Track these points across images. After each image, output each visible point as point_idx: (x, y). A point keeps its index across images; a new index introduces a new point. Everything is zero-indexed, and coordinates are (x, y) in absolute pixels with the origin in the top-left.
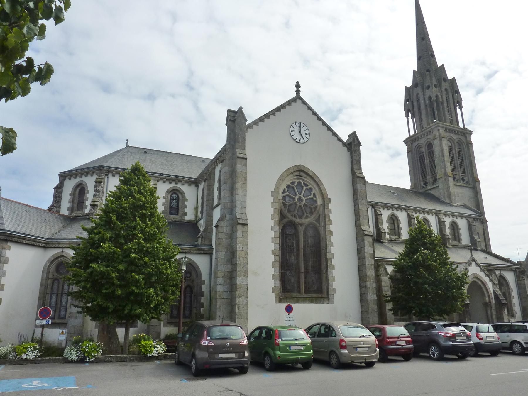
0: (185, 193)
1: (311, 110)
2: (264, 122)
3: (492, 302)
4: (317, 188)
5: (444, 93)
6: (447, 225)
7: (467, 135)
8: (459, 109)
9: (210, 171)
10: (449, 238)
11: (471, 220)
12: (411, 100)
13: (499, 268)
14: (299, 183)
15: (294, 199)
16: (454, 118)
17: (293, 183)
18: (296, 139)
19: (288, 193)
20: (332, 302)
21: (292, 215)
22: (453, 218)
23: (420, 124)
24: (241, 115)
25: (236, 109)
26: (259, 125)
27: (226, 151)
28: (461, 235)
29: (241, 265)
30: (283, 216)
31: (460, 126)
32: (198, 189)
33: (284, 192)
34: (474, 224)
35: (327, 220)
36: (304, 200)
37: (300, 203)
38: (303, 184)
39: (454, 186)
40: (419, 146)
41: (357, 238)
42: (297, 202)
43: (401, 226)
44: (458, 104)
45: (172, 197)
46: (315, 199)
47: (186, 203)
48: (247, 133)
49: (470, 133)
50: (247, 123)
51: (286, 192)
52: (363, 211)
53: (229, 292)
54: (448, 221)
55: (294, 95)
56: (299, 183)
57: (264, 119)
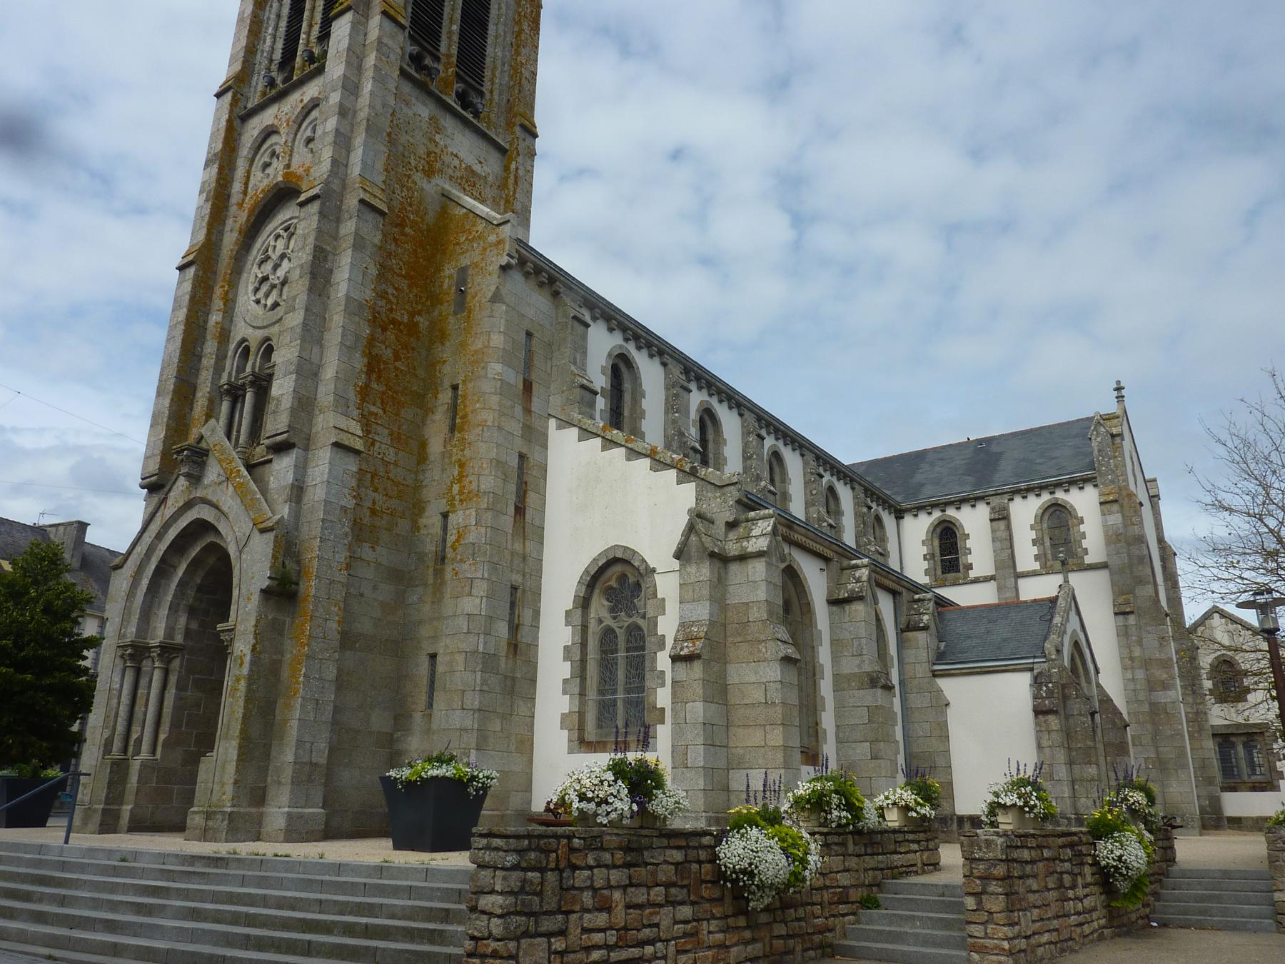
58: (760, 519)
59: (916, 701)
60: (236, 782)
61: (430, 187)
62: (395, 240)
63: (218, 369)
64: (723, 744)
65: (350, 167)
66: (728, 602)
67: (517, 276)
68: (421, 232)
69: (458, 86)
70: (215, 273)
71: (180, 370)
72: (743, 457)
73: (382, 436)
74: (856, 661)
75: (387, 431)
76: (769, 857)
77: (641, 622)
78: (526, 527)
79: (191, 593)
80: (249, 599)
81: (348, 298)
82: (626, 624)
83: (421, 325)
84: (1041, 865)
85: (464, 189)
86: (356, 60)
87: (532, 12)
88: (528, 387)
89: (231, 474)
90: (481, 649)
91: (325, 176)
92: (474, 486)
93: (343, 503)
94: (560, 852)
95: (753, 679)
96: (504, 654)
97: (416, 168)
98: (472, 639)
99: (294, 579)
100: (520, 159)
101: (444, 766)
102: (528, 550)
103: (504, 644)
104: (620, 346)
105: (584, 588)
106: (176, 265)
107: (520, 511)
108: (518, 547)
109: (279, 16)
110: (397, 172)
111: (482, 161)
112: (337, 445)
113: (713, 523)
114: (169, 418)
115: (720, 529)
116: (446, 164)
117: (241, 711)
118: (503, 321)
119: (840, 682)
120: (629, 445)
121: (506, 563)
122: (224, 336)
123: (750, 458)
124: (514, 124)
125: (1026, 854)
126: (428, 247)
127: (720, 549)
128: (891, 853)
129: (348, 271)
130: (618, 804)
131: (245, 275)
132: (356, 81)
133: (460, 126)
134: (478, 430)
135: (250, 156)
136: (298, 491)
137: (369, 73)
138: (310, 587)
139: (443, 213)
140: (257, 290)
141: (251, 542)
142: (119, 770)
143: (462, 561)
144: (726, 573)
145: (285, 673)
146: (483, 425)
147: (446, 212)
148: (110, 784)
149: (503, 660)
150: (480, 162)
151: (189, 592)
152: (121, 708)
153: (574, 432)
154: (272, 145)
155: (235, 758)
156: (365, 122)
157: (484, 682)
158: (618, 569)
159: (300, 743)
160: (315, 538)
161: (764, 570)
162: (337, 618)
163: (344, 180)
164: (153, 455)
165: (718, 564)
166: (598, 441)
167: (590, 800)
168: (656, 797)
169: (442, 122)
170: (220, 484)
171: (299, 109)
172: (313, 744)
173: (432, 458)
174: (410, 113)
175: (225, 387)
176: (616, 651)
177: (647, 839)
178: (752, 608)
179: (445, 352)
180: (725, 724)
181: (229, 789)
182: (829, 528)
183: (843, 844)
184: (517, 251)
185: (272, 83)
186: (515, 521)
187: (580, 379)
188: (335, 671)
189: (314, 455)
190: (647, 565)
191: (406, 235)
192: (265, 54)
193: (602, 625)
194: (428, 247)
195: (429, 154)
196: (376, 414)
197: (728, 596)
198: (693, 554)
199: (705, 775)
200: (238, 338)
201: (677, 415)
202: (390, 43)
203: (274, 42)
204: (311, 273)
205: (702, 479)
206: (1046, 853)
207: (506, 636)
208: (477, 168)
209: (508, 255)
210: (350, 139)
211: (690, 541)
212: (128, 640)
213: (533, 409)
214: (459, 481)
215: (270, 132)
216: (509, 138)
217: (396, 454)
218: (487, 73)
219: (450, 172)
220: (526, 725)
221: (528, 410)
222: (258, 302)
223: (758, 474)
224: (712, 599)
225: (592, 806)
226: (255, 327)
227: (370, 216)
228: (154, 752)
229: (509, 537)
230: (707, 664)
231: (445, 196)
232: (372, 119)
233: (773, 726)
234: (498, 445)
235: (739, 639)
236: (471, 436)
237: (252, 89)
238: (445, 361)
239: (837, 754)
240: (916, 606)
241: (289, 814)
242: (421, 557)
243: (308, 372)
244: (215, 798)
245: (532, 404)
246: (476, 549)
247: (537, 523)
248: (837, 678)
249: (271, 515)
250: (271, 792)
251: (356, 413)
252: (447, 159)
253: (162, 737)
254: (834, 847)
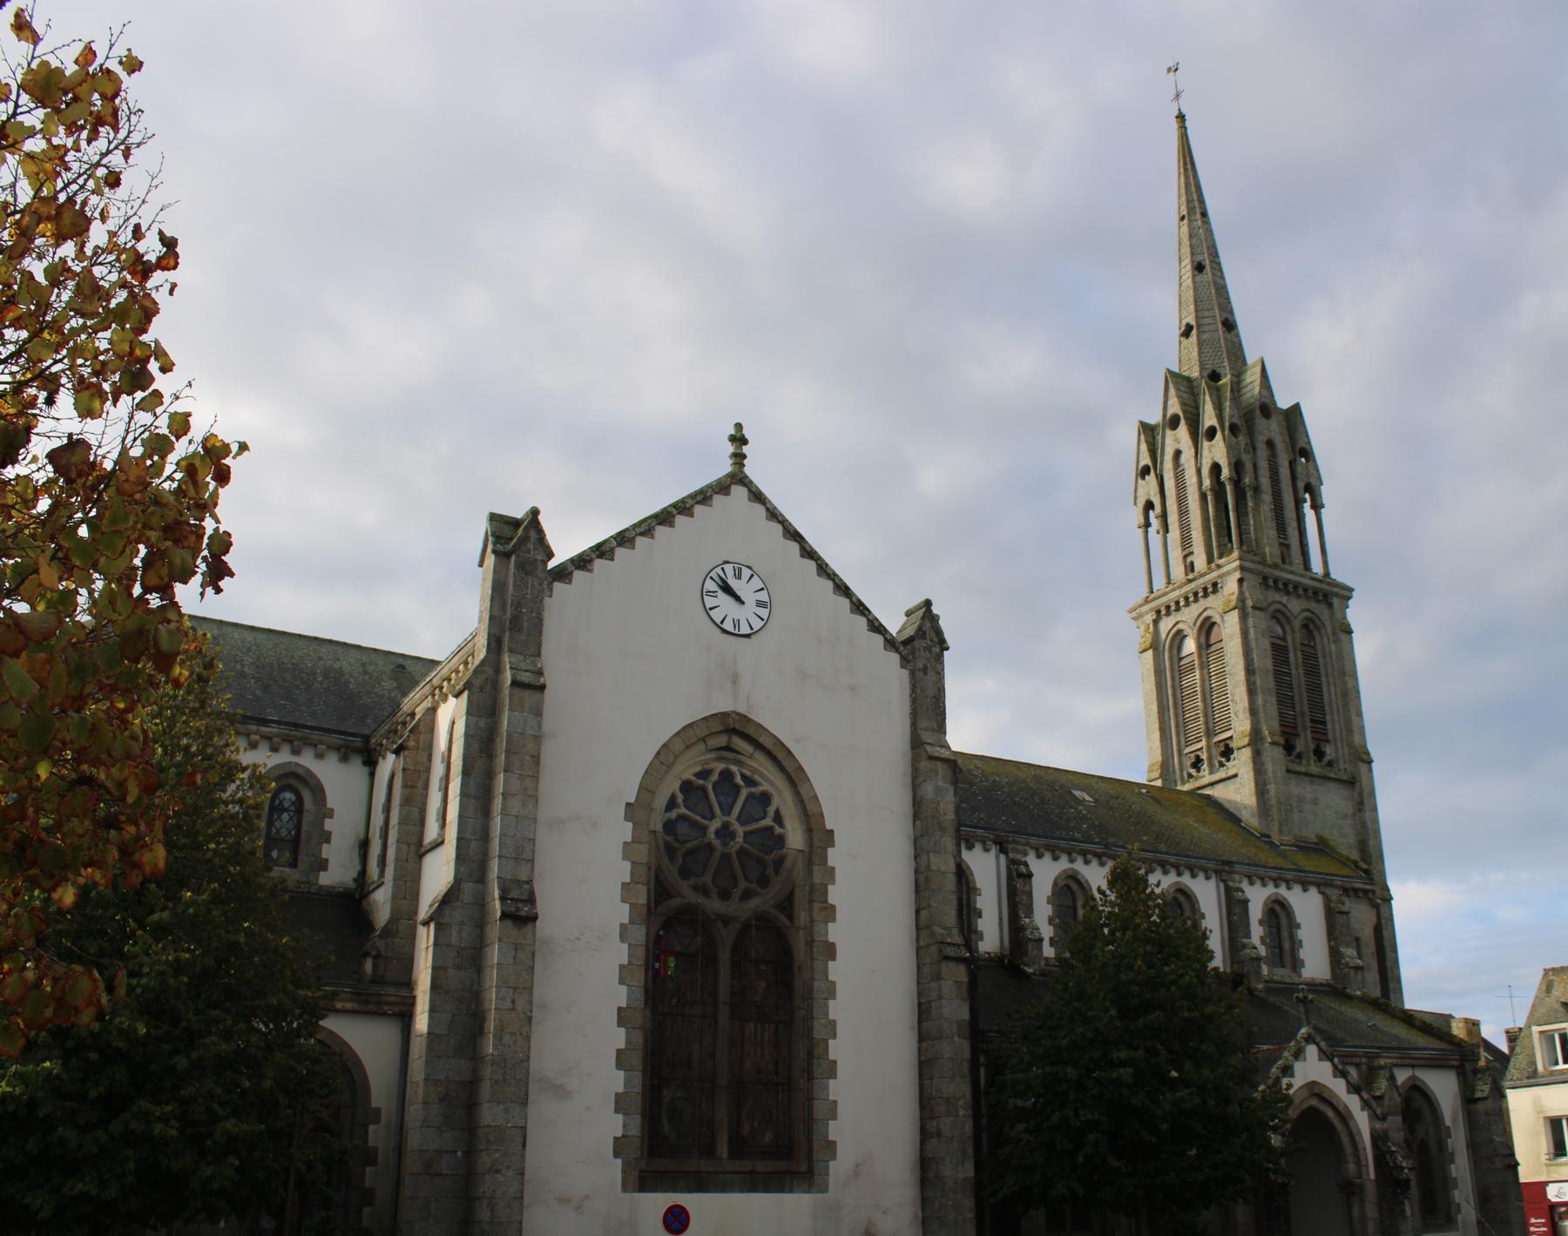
0: (326, 788)
1: (780, 522)
2: (612, 559)
3: (1365, 1177)
4: (788, 795)
5: (1263, 453)
6: (1256, 912)
7: (1336, 601)
8: (1312, 512)
9: (417, 717)
10: (1258, 959)
11: (1334, 894)
12: (1155, 470)
13: (1407, 1061)
14: (726, 775)
15: (704, 829)
16: (1294, 541)
17: (704, 774)
18: (722, 622)
19: (683, 810)
20: (824, 1189)
21: (696, 888)
22: (1277, 886)
23: (1185, 557)
24: (533, 534)
25: (518, 512)
26: (595, 571)
27: (473, 655)
28: (1301, 947)
29: (505, 1060)
30: (660, 891)
31: (1315, 570)
32: (372, 774)
33: (672, 804)
34: (1345, 909)
35: (816, 906)
36: (742, 834)
37: (725, 844)
38: (738, 780)
39: (1289, 775)
40: (1208, 618)
41: (918, 967)
42: (717, 843)
44: (1307, 496)
45: (277, 802)
46: (778, 830)
47: (328, 824)
48: (551, 596)
49: (1345, 593)
50: (552, 564)
51: (678, 807)
52: (943, 873)
53: (459, 1154)
54: (1257, 897)
55: (726, 467)
56: (726, 775)
57: (612, 550)
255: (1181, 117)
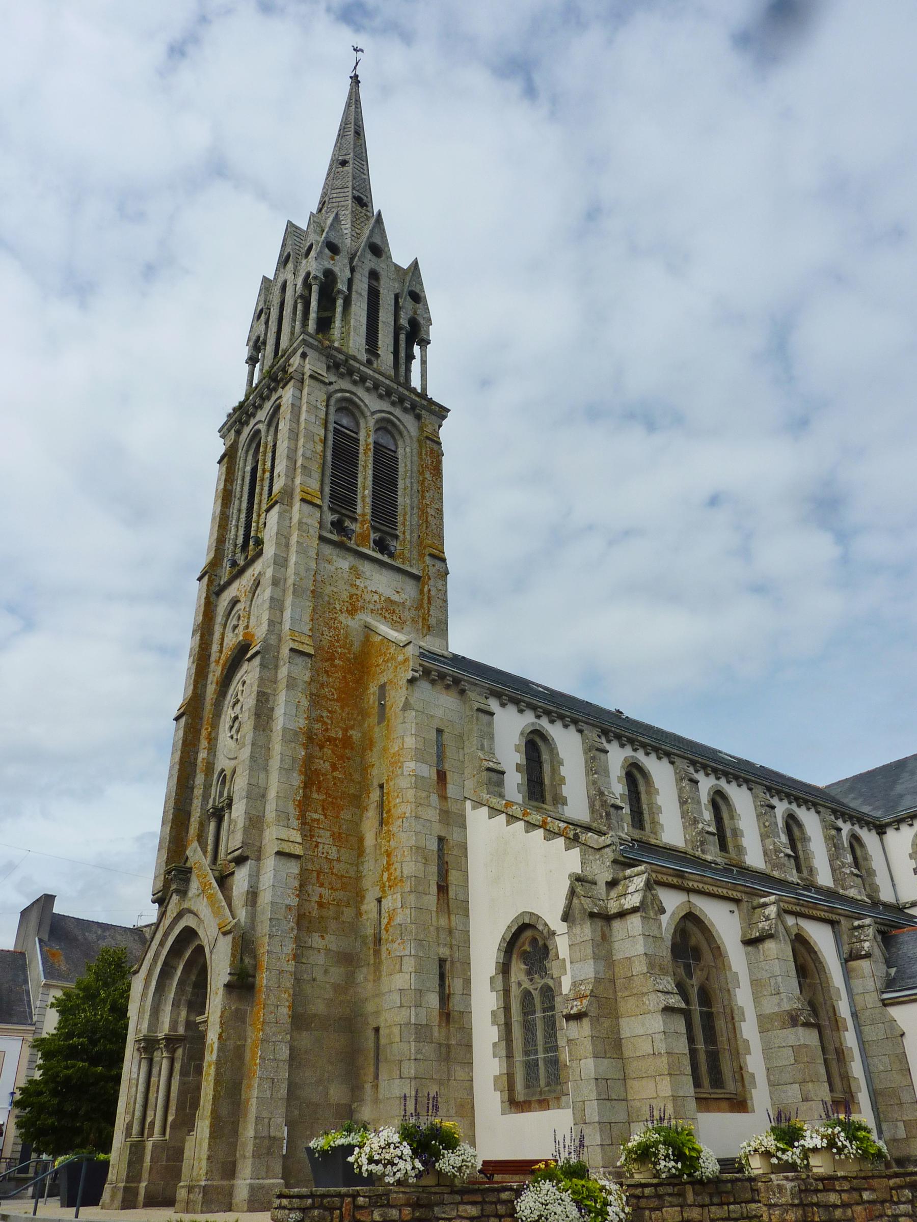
43: (564, 771)
49: (441, 412)
58: (635, 876)
59: (872, 1033)
60: (209, 1158)
61: (353, 623)
62: (327, 672)
63: (206, 796)
64: (622, 1098)
65: (283, 624)
66: (614, 958)
67: (424, 685)
68: (349, 660)
69: (373, 536)
70: (201, 719)
71: (177, 802)
72: (680, 802)
73: (324, 837)
74: (775, 999)
75: (328, 834)
76: (559, 1209)
77: (551, 983)
78: (450, 904)
79: (189, 989)
80: (217, 993)
81: (285, 730)
82: (539, 986)
83: (354, 737)
84: (859, 1209)
85: (385, 617)
86: (284, 540)
87: (433, 462)
88: (442, 777)
89: (205, 887)
90: (413, 1021)
91: (264, 635)
92: (398, 873)
93: (288, 902)
94: (344, 1209)
95: (641, 1032)
96: (436, 1023)
97: (340, 611)
98: (405, 1012)
99: (251, 972)
100: (431, 582)
101: (352, 1134)
102: (453, 924)
103: (436, 1013)
104: (533, 724)
105: (502, 954)
106: (173, 717)
107: (443, 889)
108: (443, 922)
109: (239, 511)
110: (325, 618)
111: (400, 590)
112: (279, 853)
113: (596, 884)
114: (170, 842)
115: (602, 888)
116: (367, 601)
117: (212, 1093)
118: (413, 725)
119: (765, 1023)
120: (526, 819)
121: (432, 938)
122: (209, 767)
123: (686, 802)
124: (425, 555)
125: (833, 1198)
126: (356, 672)
127: (601, 907)
128: (747, 1202)
129: (283, 708)
130: (402, 1165)
131: (223, 716)
132: (285, 556)
133: (377, 567)
134: (399, 822)
135: (223, 622)
136: (253, 896)
137: (293, 548)
138: (263, 979)
139: (367, 641)
140: (231, 727)
141: (218, 944)
142: (136, 1150)
143: (393, 941)
144: (611, 930)
145: (248, 1055)
146: (403, 817)
147: (368, 640)
148: (130, 1164)
149: (436, 1029)
150: (398, 592)
151: (187, 989)
152: (138, 1095)
153: (485, 810)
154: (238, 611)
155: (208, 1135)
156: (292, 587)
157: (418, 1051)
158: (528, 933)
159: (258, 1118)
160: (266, 935)
161: (640, 925)
162: (287, 1004)
163: (280, 635)
164: (160, 874)
165: (599, 923)
166: (503, 816)
167: (377, 1162)
168: (444, 1157)
169: (361, 568)
170: (198, 895)
171: (252, 581)
172: (270, 1119)
173: (368, 851)
174: (333, 568)
175: (211, 811)
176: (534, 1012)
177: (438, 1196)
178: (634, 962)
179: (373, 757)
180: (623, 1077)
181: (204, 1163)
182: (786, 858)
183: (681, 1194)
184: (421, 665)
185: (234, 564)
186: (438, 899)
187: (486, 763)
188: (288, 1052)
189: (263, 863)
190: (549, 928)
191: (335, 666)
192: (231, 541)
193: (521, 989)
194: (356, 672)
195: (351, 597)
196: (319, 820)
197: (614, 952)
198: (576, 916)
199: (601, 1130)
200: (219, 769)
201: (596, 776)
202: (309, 521)
203: (237, 531)
204: (256, 714)
205: (584, 844)
206: (866, 1196)
207: (438, 1007)
208: (396, 598)
209: (413, 670)
210: (283, 601)
211: (573, 904)
212: (141, 1036)
213: (449, 795)
214: (388, 869)
215: (235, 602)
216: (421, 566)
217: (338, 851)
218: (400, 519)
219: (371, 606)
220: (465, 1089)
221: (443, 797)
222: (232, 737)
223: (695, 817)
224: (596, 958)
225: (380, 1167)
226: (230, 759)
227: (300, 660)
228: (164, 1133)
229: (434, 914)
230: (596, 1021)
231: (367, 627)
232: (297, 583)
233: (661, 1077)
234: (417, 833)
235: (627, 994)
236: (394, 828)
237: (223, 570)
238: (373, 765)
239: (771, 1099)
240: (856, 934)
241: (251, 1186)
242: (364, 938)
243: (257, 795)
244: (194, 1174)
245: (448, 791)
246: (403, 929)
247: (461, 897)
248: (761, 1018)
249: (231, 919)
250: (239, 1166)
251: (296, 823)
252: (367, 597)
253: (170, 1118)
254: (667, 1198)
255: (355, 80)
